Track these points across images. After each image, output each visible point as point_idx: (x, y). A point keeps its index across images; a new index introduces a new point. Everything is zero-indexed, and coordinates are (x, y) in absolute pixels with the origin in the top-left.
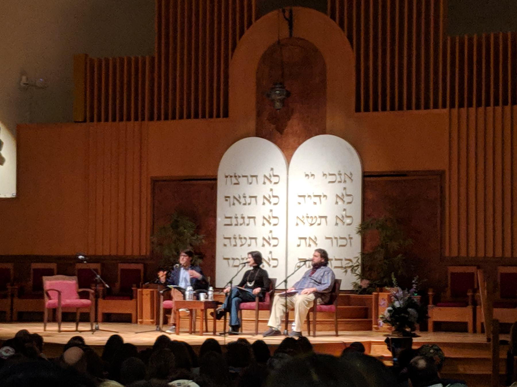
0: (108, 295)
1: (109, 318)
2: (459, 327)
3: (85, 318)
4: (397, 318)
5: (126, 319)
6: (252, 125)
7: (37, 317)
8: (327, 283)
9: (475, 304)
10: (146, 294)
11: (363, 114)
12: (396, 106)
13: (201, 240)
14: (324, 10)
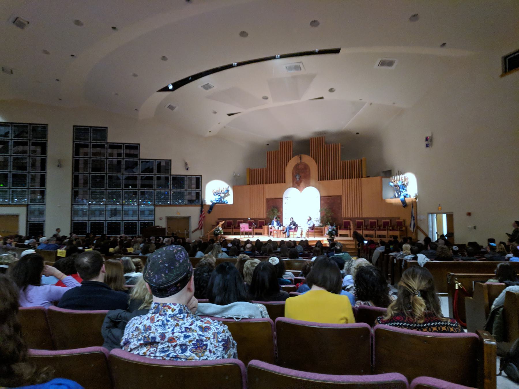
0: (256, 228)
1: (256, 234)
2: (346, 236)
3: (250, 234)
4: (330, 234)
5: (260, 234)
6: (291, 184)
7: (238, 234)
8: (312, 225)
9: (350, 229)
10: (265, 227)
11: (320, 181)
12: (328, 179)
13: (279, 214)
14: (309, 155)
